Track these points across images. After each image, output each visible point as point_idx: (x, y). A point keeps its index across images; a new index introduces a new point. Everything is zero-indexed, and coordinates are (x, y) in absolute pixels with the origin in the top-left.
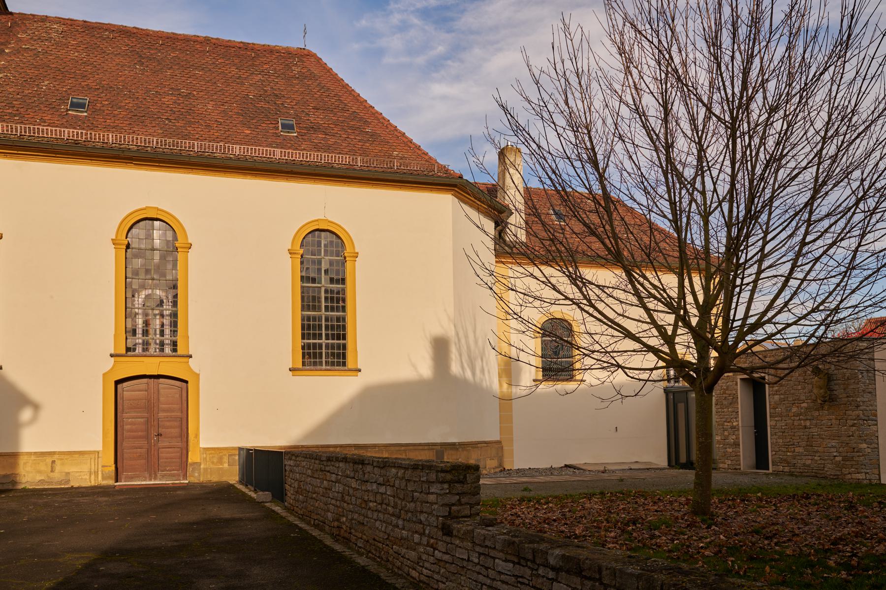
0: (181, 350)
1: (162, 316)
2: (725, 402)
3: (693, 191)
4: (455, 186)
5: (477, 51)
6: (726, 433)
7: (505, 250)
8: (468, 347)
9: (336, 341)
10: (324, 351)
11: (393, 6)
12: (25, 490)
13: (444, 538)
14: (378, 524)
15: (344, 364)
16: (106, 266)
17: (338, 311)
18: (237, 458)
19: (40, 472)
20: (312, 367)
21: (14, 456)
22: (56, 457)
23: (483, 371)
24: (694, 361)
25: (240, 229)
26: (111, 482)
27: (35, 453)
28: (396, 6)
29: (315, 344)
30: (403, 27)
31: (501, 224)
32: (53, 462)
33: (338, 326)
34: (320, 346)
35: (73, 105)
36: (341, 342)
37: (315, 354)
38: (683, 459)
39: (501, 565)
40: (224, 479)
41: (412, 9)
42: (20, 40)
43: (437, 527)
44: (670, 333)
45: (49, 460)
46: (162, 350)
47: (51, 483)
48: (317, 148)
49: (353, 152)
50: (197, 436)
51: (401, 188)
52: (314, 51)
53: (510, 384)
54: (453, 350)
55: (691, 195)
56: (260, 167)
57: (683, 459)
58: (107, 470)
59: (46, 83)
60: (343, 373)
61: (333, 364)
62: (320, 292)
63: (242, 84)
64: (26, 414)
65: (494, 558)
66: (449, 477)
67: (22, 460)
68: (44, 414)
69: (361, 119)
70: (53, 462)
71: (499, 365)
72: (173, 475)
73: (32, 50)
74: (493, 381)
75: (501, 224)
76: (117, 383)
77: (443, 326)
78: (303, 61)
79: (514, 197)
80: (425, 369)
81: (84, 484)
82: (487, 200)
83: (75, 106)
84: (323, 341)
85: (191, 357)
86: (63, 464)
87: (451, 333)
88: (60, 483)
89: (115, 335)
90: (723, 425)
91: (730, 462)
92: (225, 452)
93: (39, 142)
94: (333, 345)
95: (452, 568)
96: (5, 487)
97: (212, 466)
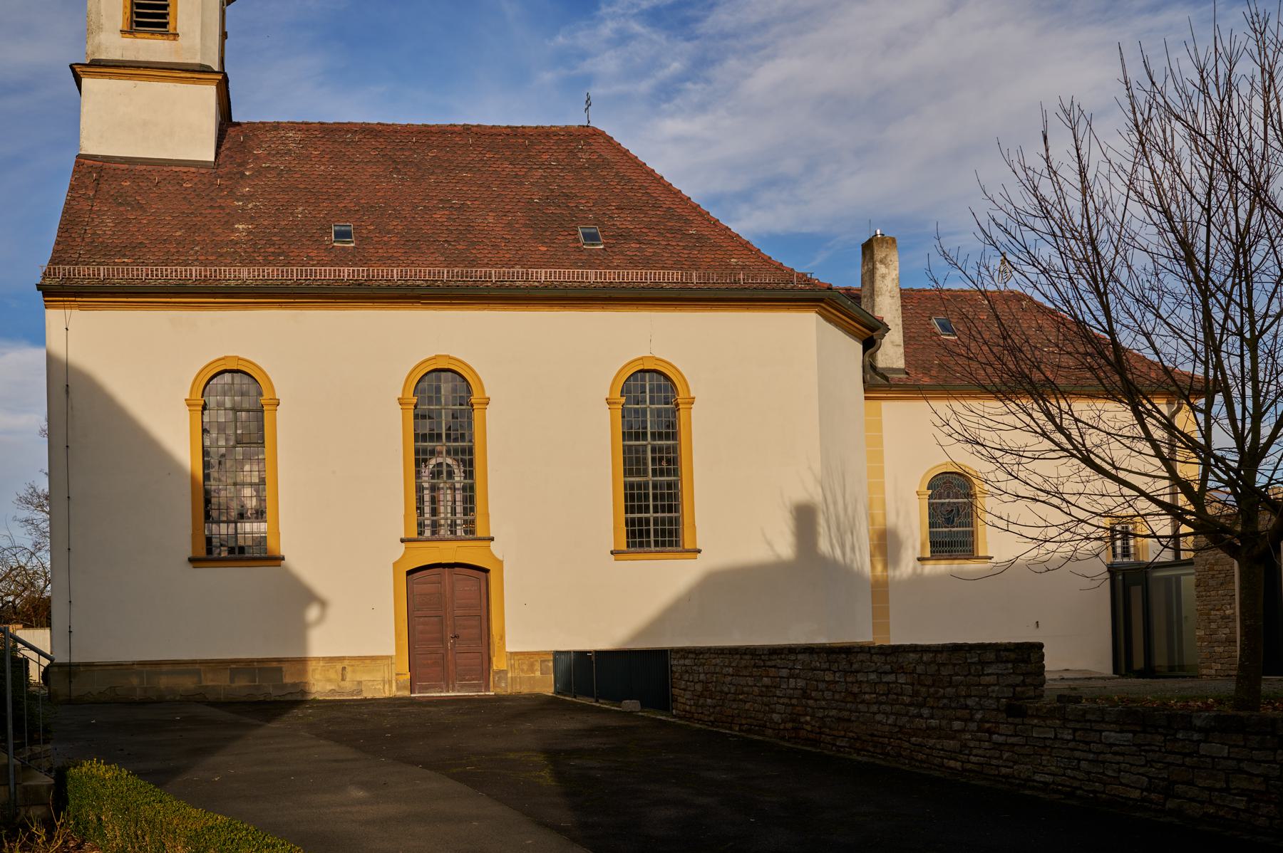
0: (480, 533)
1: (454, 489)
2: (1211, 582)
3: (1228, 305)
4: (821, 300)
5: (732, 63)
6: (1213, 626)
7: (878, 383)
8: (837, 518)
9: (666, 515)
10: (652, 527)
11: (605, 10)
12: (315, 701)
13: (1010, 720)
14: (878, 717)
15: (677, 544)
16: (392, 435)
17: (669, 475)
18: (551, 664)
19: (329, 680)
20: (638, 549)
21: (303, 661)
22: (346, 663)
23: (853, 549)
24: (1260, 528)
25: (548, 374)
26: (406, 693)
27: (324, 658)
28: (610, 10)
29: (640, 520)
30: (622, 39)
31: (870, 345)
32: (344, 669)
33: (669, 495)
34: (647, 520)
35: (338, 234)
36: (673, 515)
37: (641, 531)
38: (1139, 663)
39: (1112, 736)
40: (537, 690)
41: (635, 11)
42: (257, 157)
43: (998, 710)
44: (1196, 488)
45: (339, 666)
46: (453, 532)
47: (342, 693)
48: (633, 263)
49: (678, 265)
50: (502, 638)
51: (748, 308)
52: (601, 128)
53: (885, 566)
54: (821, 521)
55: (1226, 310)
56: (571, 294)
57: (1139, 663)
58: (402, 678)
59: (300, 209)
60: (678, 555)
61: (663, 544)
62: (645, 452)
63: (522, 184)
64: (313, 613)
65: (1101, 732)
66: (1013, 656)
67: (311, 666)
68: (332, 612)
69: (680, 217)
70: (344, 669)
71: (871, 539)
72: (475, 686)
73: (273, 169)
74: (863, 561)
75: (870, 345)
76: (409, 573)
77: (806, 489)
78: (589, 144)
79: (888, 308)
80: (784, 547)
81: (377, 696)
82: (850, 312)
83: (342, 235)
84: (651, 515)
85: (492, 539)
86: (353, 671)
87: (818, 498)
88: (352, 694)
89: (405, 516)
90: (1208, 614)
91: (1219, 666)
92: (536, 657)
93: (319, 287)
94: (663, 519)
95: (1026, 750)
96: (294, 698)
97: (522, 675)
